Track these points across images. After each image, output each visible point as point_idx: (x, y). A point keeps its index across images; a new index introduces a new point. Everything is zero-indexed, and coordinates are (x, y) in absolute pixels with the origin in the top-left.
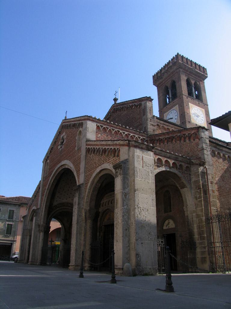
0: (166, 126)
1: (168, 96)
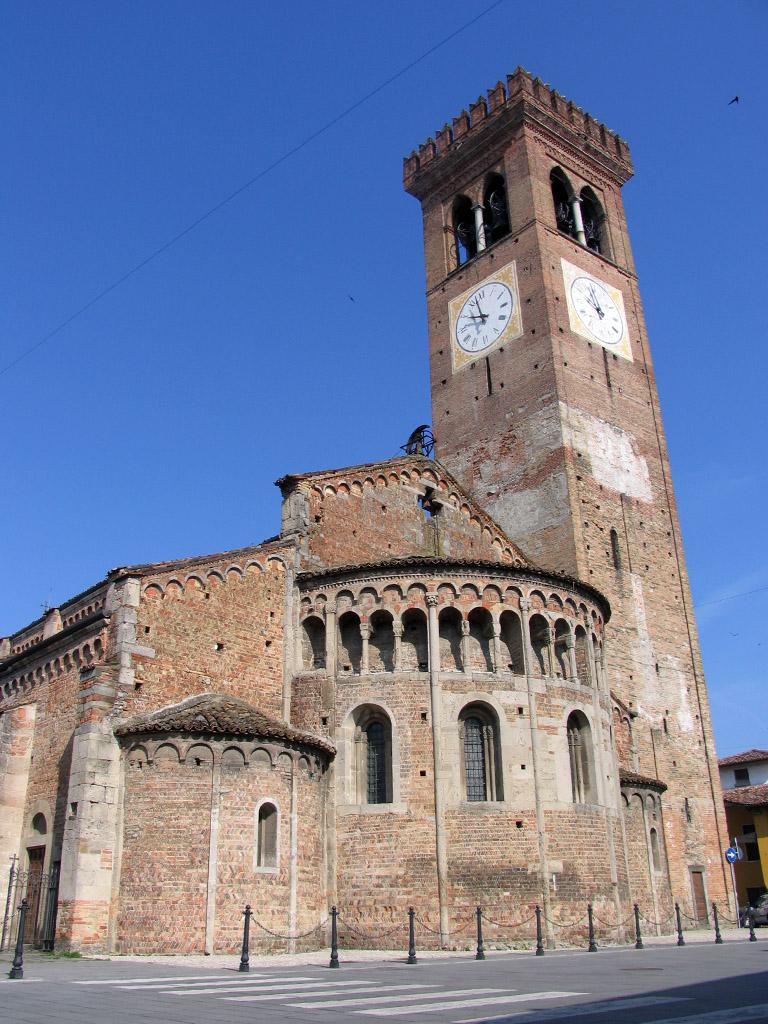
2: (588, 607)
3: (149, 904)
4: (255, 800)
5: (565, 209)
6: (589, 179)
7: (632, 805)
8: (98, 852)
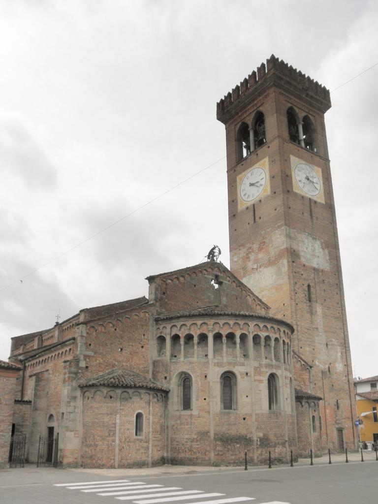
1: (244, 144)
2: (281, 329)
3: (93, 450)
4: (134, 411)
5: (294, 128)
6: (307, 111)
7: (305, 407)
8: (73, 431)
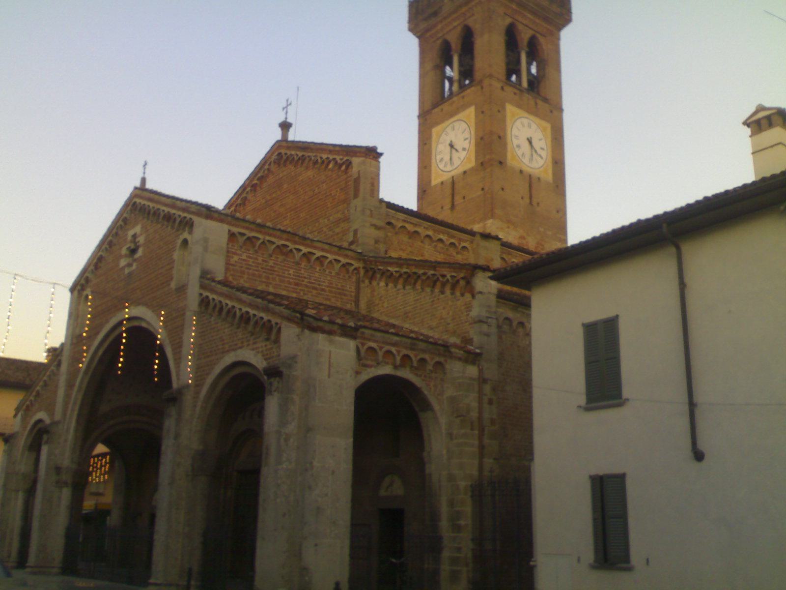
0: (412, 226)
